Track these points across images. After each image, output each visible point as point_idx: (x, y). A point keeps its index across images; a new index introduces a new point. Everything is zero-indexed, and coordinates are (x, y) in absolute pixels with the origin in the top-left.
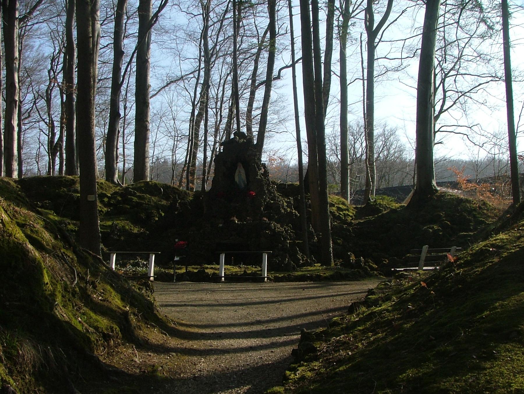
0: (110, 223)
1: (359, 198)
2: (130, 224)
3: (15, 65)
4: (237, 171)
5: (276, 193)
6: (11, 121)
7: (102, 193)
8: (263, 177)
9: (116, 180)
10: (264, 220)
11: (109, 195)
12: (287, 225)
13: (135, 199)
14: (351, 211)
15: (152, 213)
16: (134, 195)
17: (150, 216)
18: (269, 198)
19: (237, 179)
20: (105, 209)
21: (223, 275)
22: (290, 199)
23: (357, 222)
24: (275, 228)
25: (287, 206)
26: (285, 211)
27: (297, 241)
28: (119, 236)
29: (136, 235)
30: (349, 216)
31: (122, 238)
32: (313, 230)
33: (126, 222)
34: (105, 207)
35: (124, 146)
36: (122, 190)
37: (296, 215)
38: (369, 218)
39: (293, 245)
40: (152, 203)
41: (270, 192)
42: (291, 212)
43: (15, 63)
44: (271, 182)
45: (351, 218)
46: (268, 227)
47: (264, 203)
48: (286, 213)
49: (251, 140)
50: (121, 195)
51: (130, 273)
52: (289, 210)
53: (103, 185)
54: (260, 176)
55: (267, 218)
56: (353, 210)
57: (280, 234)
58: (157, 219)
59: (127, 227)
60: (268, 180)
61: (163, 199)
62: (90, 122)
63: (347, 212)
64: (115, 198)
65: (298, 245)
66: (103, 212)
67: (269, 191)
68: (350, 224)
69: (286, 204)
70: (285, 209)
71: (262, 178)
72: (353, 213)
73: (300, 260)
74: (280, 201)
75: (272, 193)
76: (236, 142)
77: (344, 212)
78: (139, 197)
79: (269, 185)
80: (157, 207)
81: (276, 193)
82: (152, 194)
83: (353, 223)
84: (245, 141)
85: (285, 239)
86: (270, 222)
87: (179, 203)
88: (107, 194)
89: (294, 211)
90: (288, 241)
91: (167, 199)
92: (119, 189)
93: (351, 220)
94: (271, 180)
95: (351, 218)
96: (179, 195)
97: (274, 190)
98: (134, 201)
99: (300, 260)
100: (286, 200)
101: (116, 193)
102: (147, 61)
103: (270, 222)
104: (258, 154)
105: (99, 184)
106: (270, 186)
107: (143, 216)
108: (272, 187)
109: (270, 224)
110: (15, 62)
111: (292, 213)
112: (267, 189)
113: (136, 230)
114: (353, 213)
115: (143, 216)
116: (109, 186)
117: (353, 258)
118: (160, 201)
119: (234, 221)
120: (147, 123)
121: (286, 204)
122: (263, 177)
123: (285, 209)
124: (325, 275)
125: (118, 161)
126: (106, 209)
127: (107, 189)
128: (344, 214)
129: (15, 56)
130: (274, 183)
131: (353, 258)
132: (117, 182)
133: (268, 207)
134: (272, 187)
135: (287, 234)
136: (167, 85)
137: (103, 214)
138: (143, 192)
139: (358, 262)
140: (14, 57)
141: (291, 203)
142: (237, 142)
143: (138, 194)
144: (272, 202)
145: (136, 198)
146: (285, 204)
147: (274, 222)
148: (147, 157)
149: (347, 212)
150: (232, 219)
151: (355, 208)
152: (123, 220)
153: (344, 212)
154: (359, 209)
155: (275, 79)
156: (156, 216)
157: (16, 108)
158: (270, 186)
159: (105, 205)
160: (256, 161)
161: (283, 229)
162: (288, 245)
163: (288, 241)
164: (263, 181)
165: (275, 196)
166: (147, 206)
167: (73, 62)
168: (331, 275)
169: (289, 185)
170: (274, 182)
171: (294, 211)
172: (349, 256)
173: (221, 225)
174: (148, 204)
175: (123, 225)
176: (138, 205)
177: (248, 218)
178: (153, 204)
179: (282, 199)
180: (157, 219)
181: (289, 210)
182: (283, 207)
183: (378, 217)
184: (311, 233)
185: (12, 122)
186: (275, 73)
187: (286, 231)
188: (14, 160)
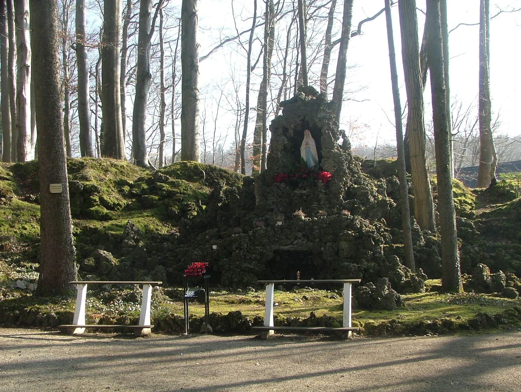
0: (125, 222)
1: (467, 178)
2: (157, 221)
3: (25, 21)
4: (304, 143)
5: (360, 173)
6: (22, 92)
7: (121, 180)
8: (341, 150)
9: (146, 162)
10: (345, 215)
11: (131, 182)
12: (379, 220)
13: (166, 187)
14: (470, 196)
15: (188, 205)
16: (166, 181)
17: (185, 210)
18: (351, 180)
19: (303, 154)
20: (124, 202)
21: (272, 324)
22: (381, 181)
23: (480, 211)
24: (361, 227)
25: (377, 192)
26: (375, 199)
27: (395, 246)
28: (137, 241)
29: (164, 238)
30: (468, 203)
31: (141, 244)
32: (419, 227)
33: (151, 218)
34: (125, 199)
35: (173, 121)
36: (150, 175)
37: (391, 205)
38: (497, 207)
39: (390, 251)
40: (190, 192)
41: (353, 173)
42: (384, 201)
43: (26, 19)
44: (354, 158)
45: (470, 207)
46: (351, 225)
47: (344, 188)
48: (376, 202)
49: (323, 95)
50: (149, 182)
51: (113, 318)
52: (380, 197)
53: (124, 168)
54: (338, 149)
55: (349, 211)
56: (471, 195)
57: (369, 235)
58: (195, 213)
59: (152, 227)
60: (349, 154)
61: (206, 185)
62: (51, 62)
63: (463, 198)
64: (139, 186)
65: (397, 251)
66: (121, 206)
67: (351, 170)
68: (470, 216)
69: (376, 189)
70: (374, 196)
71: (340, 151)
72: (472, 200)
73: (402, 276)
74: (367, 185)
75: (357, 173)
76: (302, 100)
77: (460, 198)
78: (172, 184)
79: (350, 162)
80: (196, 197)
81: (360, 173)
82: (190, 179)
83: (474, 214)
84: (314, 98)
85: (377, 242)
86: (354, 218)
87: (225, 192)
88: (128, 181)
89: (387, 199)
90: (382, 246)
91: (210, 186)
92: (147, 174)
93: (471, 209)
94: (353, 154)
95: (470, 207)
96: (228, 179)
97: (358, 170)
98: (164, 190)
99: (402, 276)
100: (376, 182)
101: (141, 179)
102: (194, 14)
103: (354, 218)
104: (334, 117)
105: (119, 168)
106: (353, 164)
107: (176, 209)
108: (356, 165)
109: (353, 220)
110: (25, 17)
111: (386, 201)
112: (348, 168)
113: (164, 230)
114: (472, 200)
115: (176, 209)
116: (134, 170)
117: (487, 273)
118: (201, 188)
119: (298, 217)
120: (196, 91)
121: (376, 189)
122: (341, 150)
123: (374, 196)
124: (459, 321)
125: (165, 140)
126: (125, 202)
127: (130, 174)
128: (460, 201)
129: (25, 10)
130: (357, 159)
131: (487, 273)
132: (148, 165)
133: (350, 194)
134: (356, 165)
135: (380, 234)
136: (221, 45)
137: (121, 209)
138: (178, 177)
139: (496, 280)
140: (24, 11)
141: (382, 187)
142: (303, 101)
143: (171, 179)
144: (356, 186)
145: (167, 186)
146: (374, 188)
147: (360, 217)
148: (197, 133)
149: (463, 198)
150: (296, 213)
151: (472, 192)
152: (147, 216)
153: (460, 198)
154: (479, 193)
155: (353, 35)
156: (194, 209)
157: (27, 75)
158: (353, 164)
159: (125, 196)
160: (331, 126)
161: (374, 227)
162: (382, 252)
163: (382, 246)
164: (341, 155)
165: (359, 177)
166: (182, 195)
167: (82, 4)
168: (470, 321)
169: (378, 162)
170: (358, 158)
171: (387, 199)
172: (482, 271)
173: (280, 223)
174: (184, 193)
175: (146, 223)
176: (170, 195)
177: (320, 211)
178: (191, 193)
179: (370, 181)
180: (195, 213)
181: (380, 197)
182: (372, 192)
183: (512, 204)
184: (415, 233)
185: (24, 93)
186: (353, 28)
187: (378, 230)
188: (27, 142)
